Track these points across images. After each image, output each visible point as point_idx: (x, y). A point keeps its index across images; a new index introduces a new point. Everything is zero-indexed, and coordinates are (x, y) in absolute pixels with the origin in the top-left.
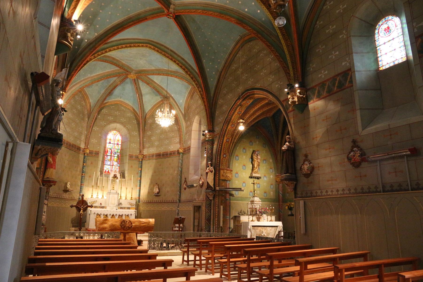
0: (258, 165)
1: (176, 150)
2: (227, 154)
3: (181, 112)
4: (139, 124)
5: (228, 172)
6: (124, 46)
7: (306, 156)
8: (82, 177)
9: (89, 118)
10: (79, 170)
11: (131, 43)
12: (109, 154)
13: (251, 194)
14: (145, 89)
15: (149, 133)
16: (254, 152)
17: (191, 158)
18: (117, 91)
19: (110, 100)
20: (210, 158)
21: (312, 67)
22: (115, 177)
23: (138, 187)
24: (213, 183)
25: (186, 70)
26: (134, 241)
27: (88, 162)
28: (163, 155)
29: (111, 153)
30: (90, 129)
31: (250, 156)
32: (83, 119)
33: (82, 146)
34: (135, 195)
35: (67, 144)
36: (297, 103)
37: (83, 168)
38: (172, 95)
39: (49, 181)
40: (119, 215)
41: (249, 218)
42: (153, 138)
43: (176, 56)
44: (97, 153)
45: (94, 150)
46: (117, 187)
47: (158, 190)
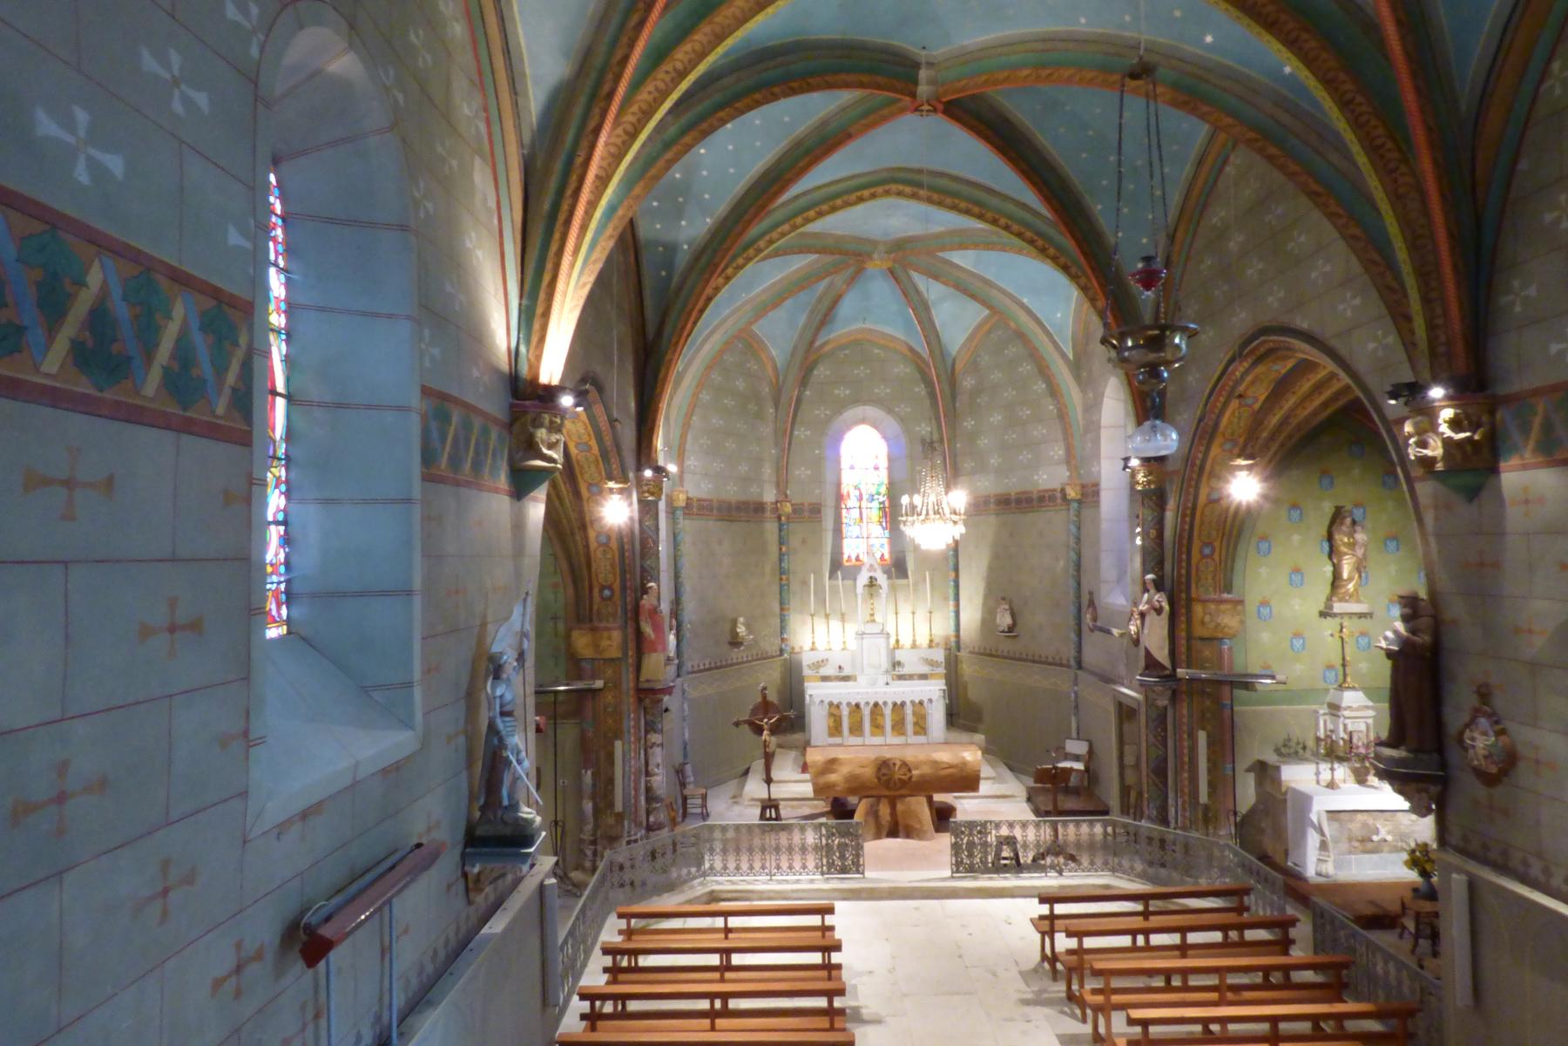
0: (1359, 568)
1: (1058, 486)
2: (1217, 544)
3: (1063, 355)
4: (932, 395)
5: (1223, 607)
6: (812, 213)
7: (1484, 694)
8: (781, 586)
9: (777, 405)
10: (768, 569)
11: (838, 195)
12: (852, 502)
13: (1331, 675)
14: (932, 290)
15: (968, 424)
16: (1337, 517)
17: (1104, 526)
18: (846, 307)
19: (832, 335)
20: (1154, 557)
21: (1522, 293)
22: (872, 583)
23: (952, 603)
24: (1166, 651)
25: (1040, 243)
26: (920, 822)
27: (795, 541)
28: (1018, 501)
29: (860, 498)
30: (785, 438)
31: (1324, 532)
32: (759, 415)
33: (769, 496)
34: (942, 627)
35: (719, 509)
36: (1439, 466)
37: (781, 561)
38: (1025, 301)
39: (653, 691)
40: (895, 704)
41: (1318, 773)
42: (983, 442)
43: (994, 201)
44: (816, 510)
45: (807, 500)
46: (882, 605)
47: (1008, 620)
